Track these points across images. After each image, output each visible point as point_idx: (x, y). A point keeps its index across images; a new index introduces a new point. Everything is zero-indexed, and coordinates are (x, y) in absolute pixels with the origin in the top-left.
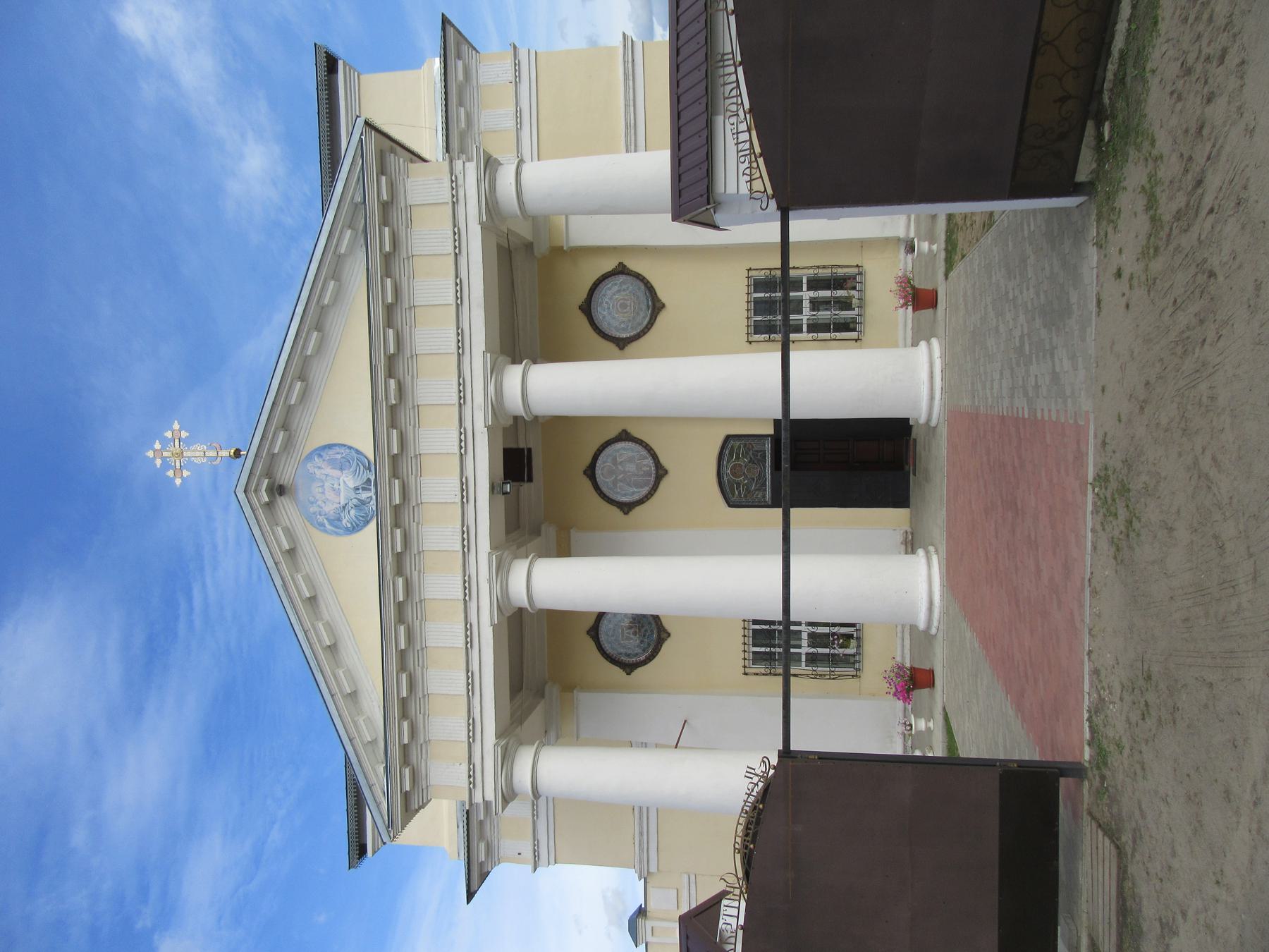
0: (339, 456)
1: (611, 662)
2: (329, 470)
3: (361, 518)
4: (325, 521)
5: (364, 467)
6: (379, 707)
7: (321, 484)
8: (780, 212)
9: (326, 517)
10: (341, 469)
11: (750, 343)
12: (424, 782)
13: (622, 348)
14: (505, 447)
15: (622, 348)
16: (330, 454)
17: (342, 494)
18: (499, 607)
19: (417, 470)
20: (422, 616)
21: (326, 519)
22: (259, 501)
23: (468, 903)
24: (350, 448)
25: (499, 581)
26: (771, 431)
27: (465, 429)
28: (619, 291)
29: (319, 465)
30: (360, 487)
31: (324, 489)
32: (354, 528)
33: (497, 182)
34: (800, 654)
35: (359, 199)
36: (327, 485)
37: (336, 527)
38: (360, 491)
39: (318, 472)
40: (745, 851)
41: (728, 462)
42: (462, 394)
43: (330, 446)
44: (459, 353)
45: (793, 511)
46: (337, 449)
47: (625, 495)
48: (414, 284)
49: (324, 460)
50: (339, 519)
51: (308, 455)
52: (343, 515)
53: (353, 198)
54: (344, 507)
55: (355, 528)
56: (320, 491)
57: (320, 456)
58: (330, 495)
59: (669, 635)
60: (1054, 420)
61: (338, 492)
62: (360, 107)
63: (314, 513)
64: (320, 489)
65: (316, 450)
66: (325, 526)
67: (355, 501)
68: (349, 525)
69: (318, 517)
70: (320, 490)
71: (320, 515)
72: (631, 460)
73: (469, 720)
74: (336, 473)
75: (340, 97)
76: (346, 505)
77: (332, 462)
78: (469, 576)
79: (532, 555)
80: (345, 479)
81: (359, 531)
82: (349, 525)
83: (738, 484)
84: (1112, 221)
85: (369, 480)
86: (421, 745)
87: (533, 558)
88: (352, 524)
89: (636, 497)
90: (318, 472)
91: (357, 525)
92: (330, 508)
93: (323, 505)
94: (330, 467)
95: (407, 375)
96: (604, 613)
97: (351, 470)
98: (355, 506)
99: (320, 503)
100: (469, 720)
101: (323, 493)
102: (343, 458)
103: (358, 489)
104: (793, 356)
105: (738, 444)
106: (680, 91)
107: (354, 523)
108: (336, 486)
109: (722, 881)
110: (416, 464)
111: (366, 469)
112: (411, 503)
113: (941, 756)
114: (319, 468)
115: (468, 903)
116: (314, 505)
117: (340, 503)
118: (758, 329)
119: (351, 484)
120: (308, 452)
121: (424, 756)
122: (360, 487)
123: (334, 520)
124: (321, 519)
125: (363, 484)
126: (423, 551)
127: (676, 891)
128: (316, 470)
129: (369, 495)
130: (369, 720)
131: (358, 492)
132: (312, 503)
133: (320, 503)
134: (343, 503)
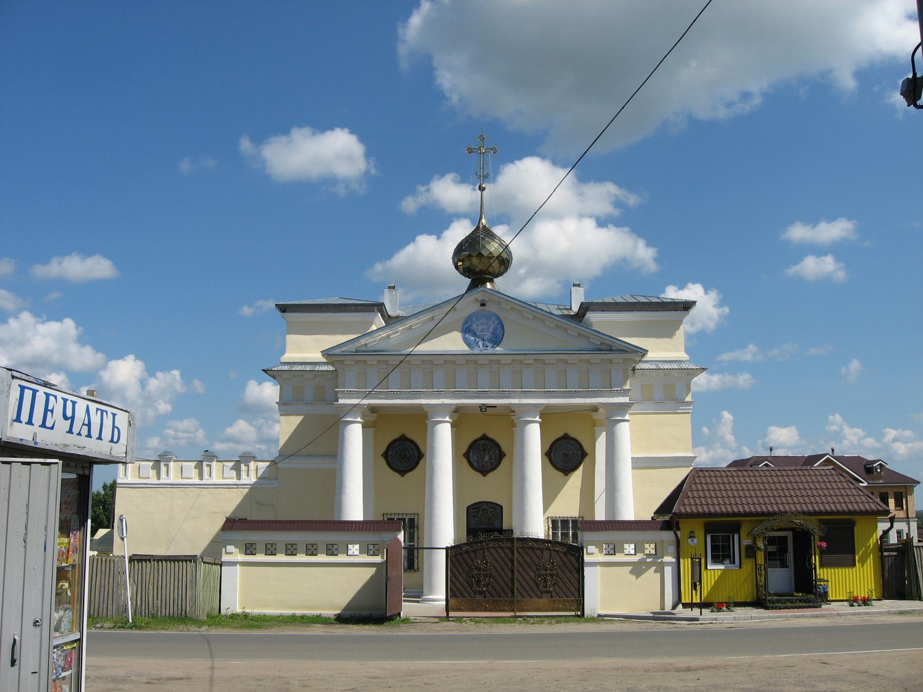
0: (498, 333)
2: (492, 327)
8: (238, 549)
10: (493, 333)
11: (548, 518)
13: (546, 454)
15: (546, 454)
16: (500, 328)
17: (481, 333)
23: (262, 370)
26: (505, 527)
28: (574, 453)
32: (465, 338)
34: (414, 542)
36: (485, 326)
40: (396, 519)
41: (489, 507)
46: (502, 332)
47: (473, 455)
57: (499, 324)
58: (481, 327)
59: (403, 476)
61: (482, 331)
63: (472, 319)
65: (502, 322)
70: (483, 323)
72: (490, 458)
74: (491, 330)
77: (495, 329)
83: (478, 512)
93: (476, 324)
99: (477, 322)
101: (481, 324)
104: (425, 547)
105: (499, 512)
106: (657, 523)
108: (484, 331)
114: (493, 323)
115: (262, 370)
118: (554, 522)
124: (470, 322)
128: (492, 321)
129: (481, 347)
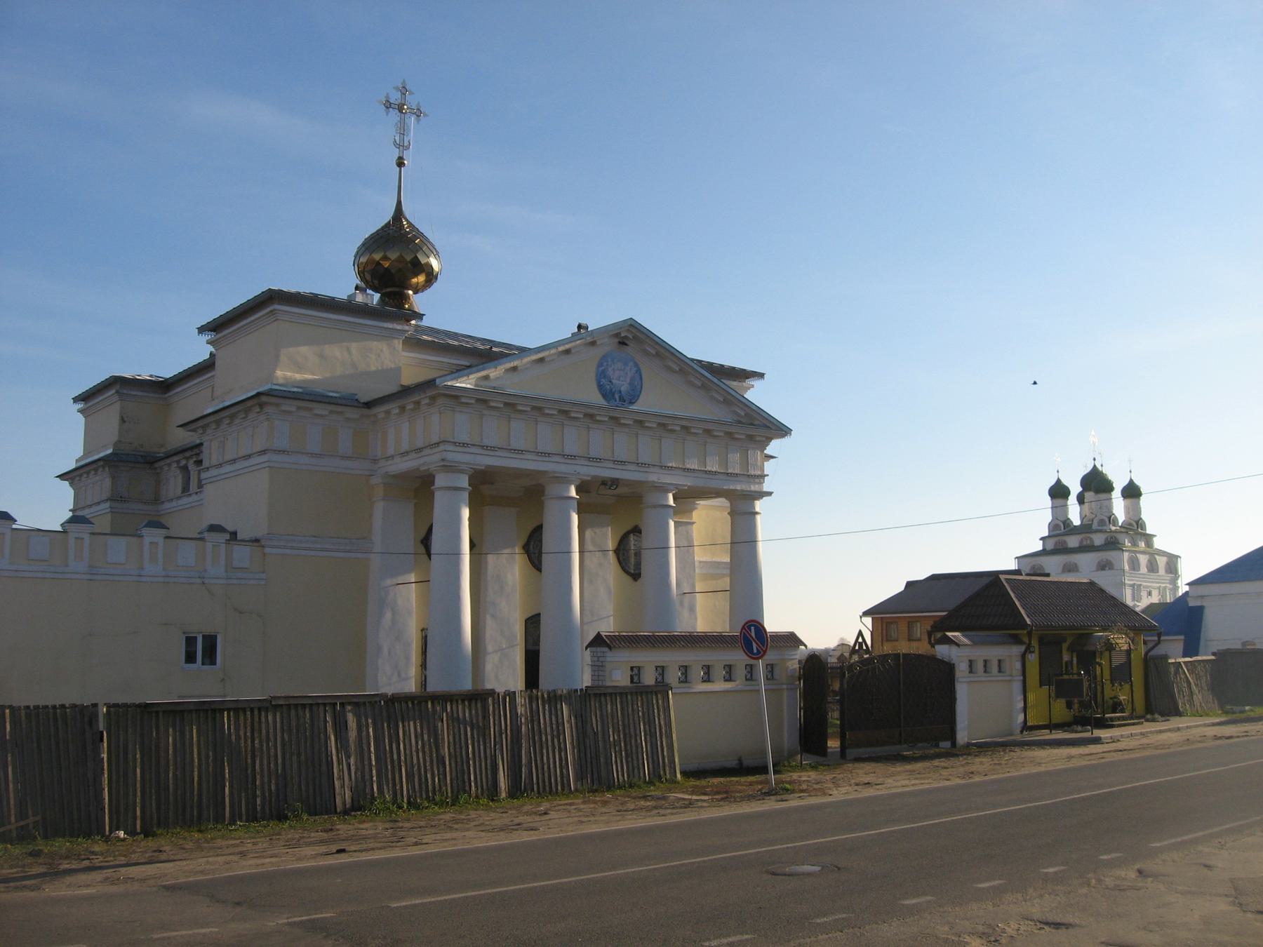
0: (636, 383)
6: (43, 536)
14: (1137, 500)
24: (640, 392)
33: (394, 392)
35: (756, 422)
39: (628, 368)
43: (641, 379)
50: (605, 377)
53: (758, 420)
54: (610, 382)
60: (820, 868)
65: (640, 370)
67: (614, 390)
68: (602, 383)
74: (628, 382)
77: (632, 379)
82: (602, 383)
84: (535, 942)
90: (628, 368)
92: (610, 372)
99: (613, 367)
113: (1014, 569)
114: (630, 370)
119: (622, 389)
124: (605, 364)
134: (613, 381)
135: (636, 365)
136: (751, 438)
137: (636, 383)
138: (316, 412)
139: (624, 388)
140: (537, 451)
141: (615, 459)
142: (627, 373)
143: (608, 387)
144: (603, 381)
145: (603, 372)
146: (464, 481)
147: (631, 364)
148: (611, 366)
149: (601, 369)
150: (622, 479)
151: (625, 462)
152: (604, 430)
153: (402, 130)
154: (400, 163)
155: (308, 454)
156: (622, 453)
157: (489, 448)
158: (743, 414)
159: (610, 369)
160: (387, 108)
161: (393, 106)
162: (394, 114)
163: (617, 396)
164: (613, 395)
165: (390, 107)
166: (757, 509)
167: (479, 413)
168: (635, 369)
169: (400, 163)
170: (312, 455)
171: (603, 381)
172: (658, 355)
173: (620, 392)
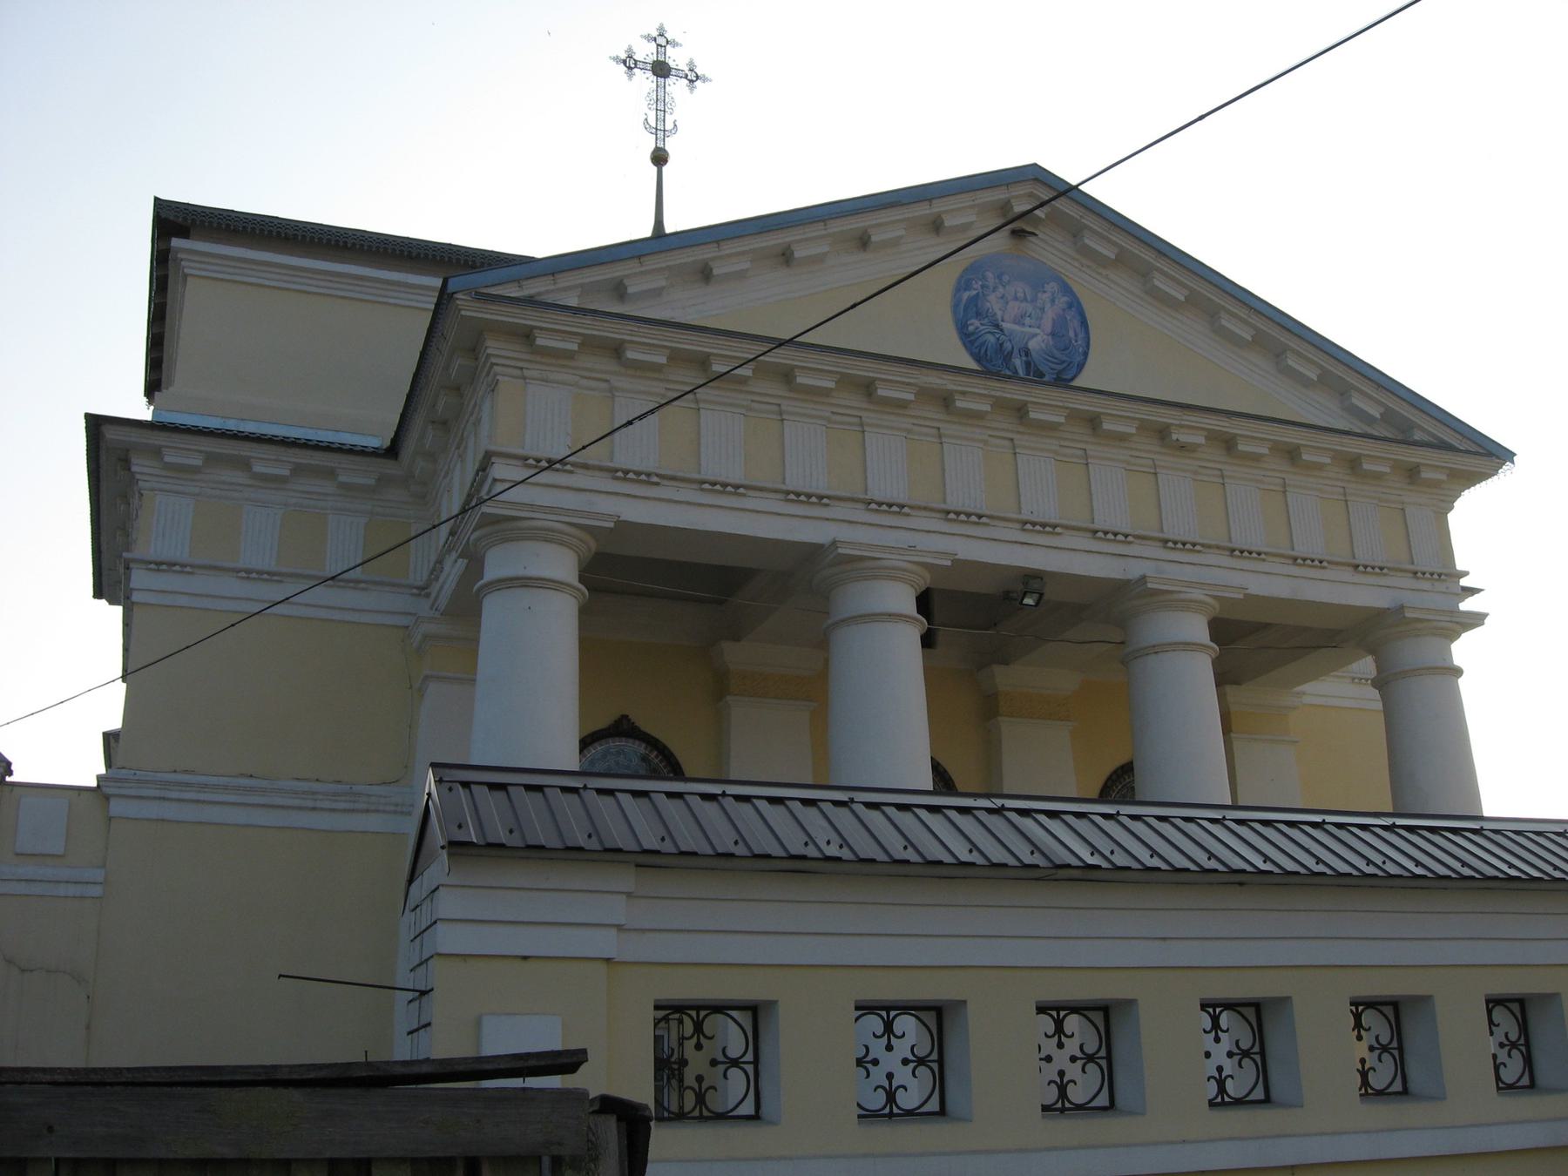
0: (1071, 334)
1: (657, 740)
3: (983, 351)
4: (975, 292)
5: (1060, 372)
7: (1029, 298)
9: (981, 295)
10: (1053, 334)
12: (535, 374)
17: (1016, 327)
18: (861, 559)
19: (1065, 455)
20: (835, 423)
21: (978, 294)
22: (1017, 197)
24: (1086, 354)
25: (909, 566)
27: (1199, 552)
29: (1057, 301)
30: (1029, 358)
31: (1022, 301)
37: (966, 309)
38: (1024, 358)
39: (1046, 297)
42: (631, 476)
43: (1084, 323)
44: (617, 471)
45: (752, 1065)
46: (1081, 335)
48: (729, 414)
49: (1064, 310)
50: (978, 315)
51: (1071, 289)
52: (986, 321)
54: (997, 326)
55: (968, 339)
56: (1018, 295)
57: (1070, 306)
58: (1014, 308)
62: (222, 280)
64: (1022, 295)
66: (965, 290)
67: (1008, 346)
68: (971, 328)
69: (980, 283)
70: (1020, 295)
71: (982, 287)
73: (657, 475)
75: (418, 277)
76: (1002, 330)
78: (908, 515)
79: (586, 591)
80: (1039, 338)
81: (964, 344)
82: (971, 328)
85: (1042, 375)
86: (607, 381)
87: (578, 590)
88: (973, 334)
89: (1152, 818)
90: (1046, 297)
91: (972, 342)
92: (993, 303)
94: (1055, 318)
95: (990, 432)
96: (932, 758)
97: (1055, 352)
98: (1001, 345)
99: (1001, 289)
100: (657, 475)
101: (1016, 299)
102: (1071, 341)
103: (1026, 355)
107: (976, 336)
109: (281, 978)
110: (850, 424)
111: (1057, 373)
112: (1019, 436)
114: (1053, 301)
116: (997, 281)
117: (1003, 321)
119: (1032, 345)
120: (1075, 290)
121: (585, 382)
122: (1029, 358)
123: (976, 306)
124: (977, 285)
125: (1035, 365)
126: (782, 420)
127: (61, 851)
130: (657, 293)
131: (1023, 354)
132: (1000, 277)
133: (1001, 289)
134: (1005, 325)
135: (1066, 289)
136: (1412, 474)
137: (1071, 334)
138: (258, 468)
139: (1038, 342)
140: (784, 487)
141: (1024, 517)
142: (1043, 310)
143: (991, 339)
144: (974, 324)
145: (974, 300)
146: (561, 564)
147: (1052, 287)
148: (995, 289)
149: (966, 295)
150: (1053, 575)
151: (1054, 526)
152: (985, 442)
153: (661, 105)
154: (660, 158)
155: (239, 571)
156: (1042, 501)
157: (631, 476)
158: (1375, 412)
159: (992, 297)
160: (630, 68)
161: (639, 64)
162: (645, 81)
163: (1018, 362)
164: (1008, 358)
165: (636, 67)
166: (1457, 660)
167: (603, 385)
168: (1065, 299)
169: (660, 158)
170: (248, 574)
171: (974, 324)
172: (1122, 261)
173: (1027, 353)
